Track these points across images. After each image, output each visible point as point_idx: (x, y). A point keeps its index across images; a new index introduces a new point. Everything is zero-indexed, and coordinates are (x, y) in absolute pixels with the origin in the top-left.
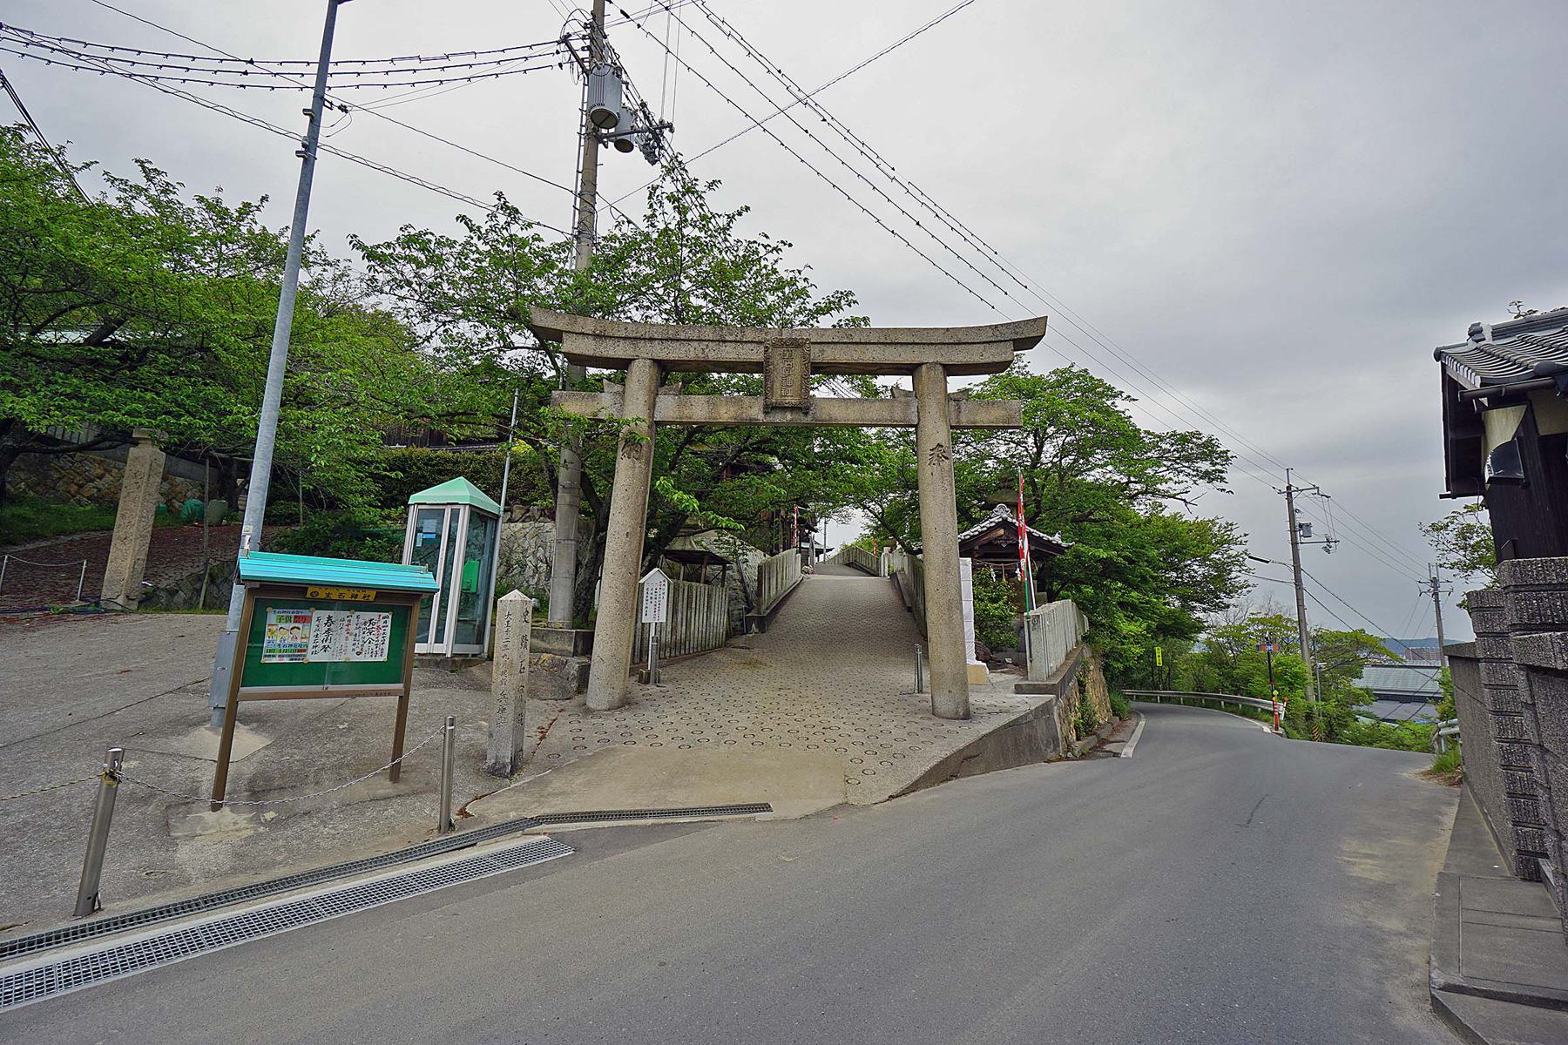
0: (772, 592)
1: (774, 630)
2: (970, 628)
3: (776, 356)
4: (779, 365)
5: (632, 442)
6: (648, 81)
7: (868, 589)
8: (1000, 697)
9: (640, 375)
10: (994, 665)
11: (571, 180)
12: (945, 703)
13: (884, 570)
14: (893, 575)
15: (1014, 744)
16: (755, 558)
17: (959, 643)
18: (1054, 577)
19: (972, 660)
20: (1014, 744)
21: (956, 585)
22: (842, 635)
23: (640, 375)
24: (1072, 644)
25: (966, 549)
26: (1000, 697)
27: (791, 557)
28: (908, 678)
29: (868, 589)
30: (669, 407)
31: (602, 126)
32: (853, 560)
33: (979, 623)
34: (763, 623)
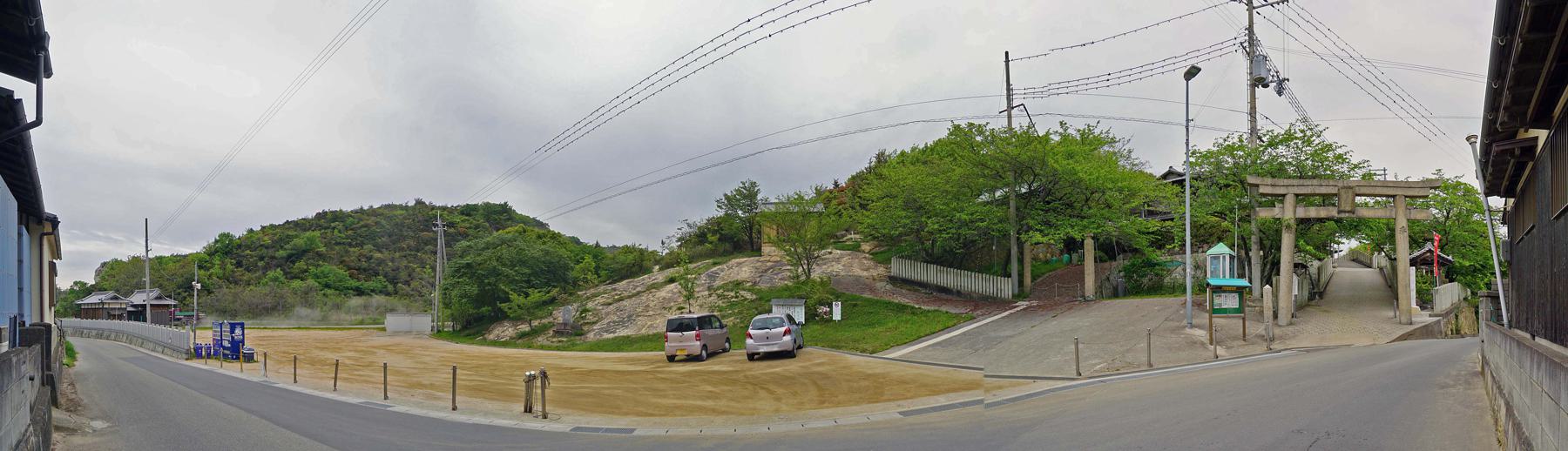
0: (1323, 279)
1: (1326, 298)
2: (1414, 294)
3: (1343, 192)
4: (1343, 195)
5: (1288, 227)
6: (1278, 62)
7: (1367, 275)
8: (1423, 318)
9: (1290, 200)
10: (1423, 308)
11: (1246, 108)
12: (1404, 319)
13: (1375, 264)
14: (1381, 269)
15: (1427, 332)
16: (1316, 263)
17: (1409, 299)
18: (1451, 274)
19: (1414, 305)
20: (1427, 332)
21: (1409, 278)
22: (1357, 300)
23: (1290, 200)
24: (1456, 300)
25: (1413, 262)
26: (1423, 318)
27: (1328, 260)
28: (1391, 314)
29: (1367, 275)
30: (1302, 213)
31: (1258, 82)
32: (1355, 258)
33: (1418, 292)
34: (1321, 295)
